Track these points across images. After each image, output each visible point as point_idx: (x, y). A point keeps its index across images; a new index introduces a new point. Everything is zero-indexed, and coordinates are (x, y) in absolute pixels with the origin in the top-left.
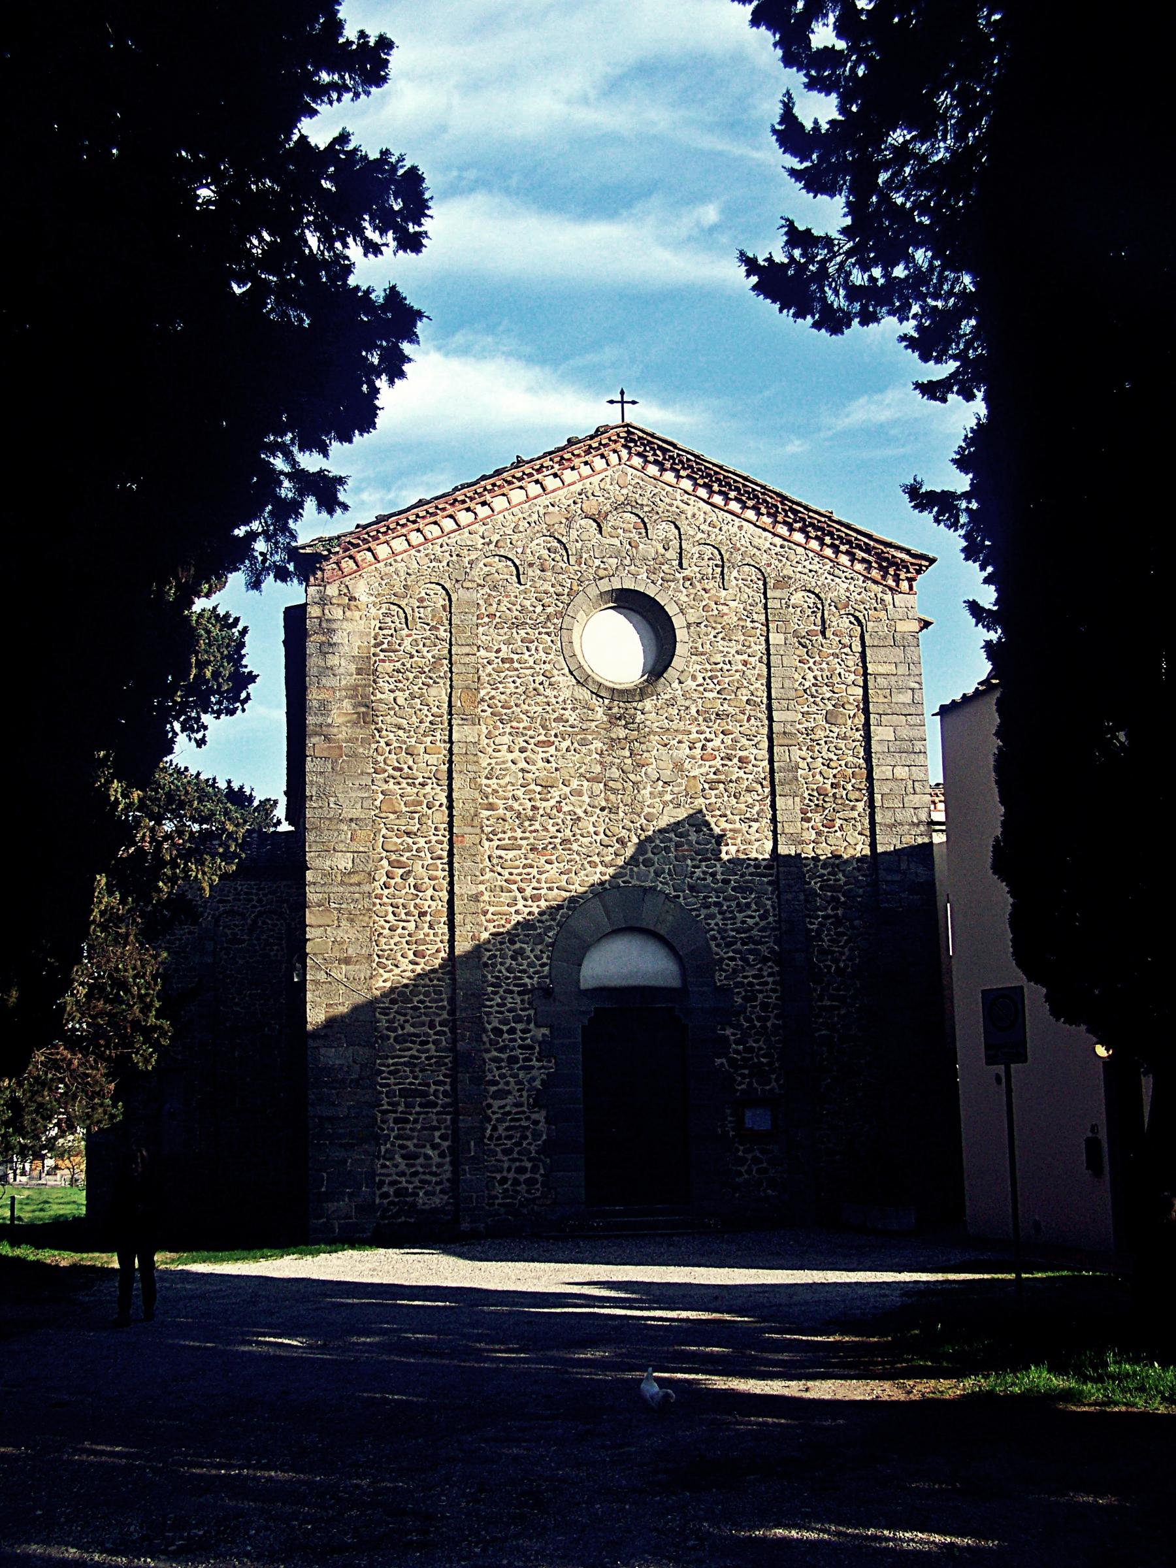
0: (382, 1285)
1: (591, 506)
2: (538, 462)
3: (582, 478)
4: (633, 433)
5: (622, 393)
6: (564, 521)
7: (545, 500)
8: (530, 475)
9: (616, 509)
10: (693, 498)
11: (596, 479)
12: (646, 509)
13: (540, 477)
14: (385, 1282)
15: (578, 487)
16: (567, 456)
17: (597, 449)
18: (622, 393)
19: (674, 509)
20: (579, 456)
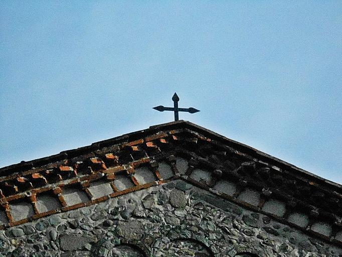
0: (105, 141)
1: (130, 230)
2: (51, 165)
3: (117, 194)
4: (193, 135)
5: (176, 99)
6: (89, 247)
7: (61, 219)
8: (39, 183)
9: (168, 234)
10: (283, 226)
11: (137, 197)
12: (214, 236)
13: (55, 186)
14: (106, 139)
15: (114, 204)
16: (94, 160)
17: (138, 155)
18: (176, 99)
19: (255, 238)
20: (110, 163)
